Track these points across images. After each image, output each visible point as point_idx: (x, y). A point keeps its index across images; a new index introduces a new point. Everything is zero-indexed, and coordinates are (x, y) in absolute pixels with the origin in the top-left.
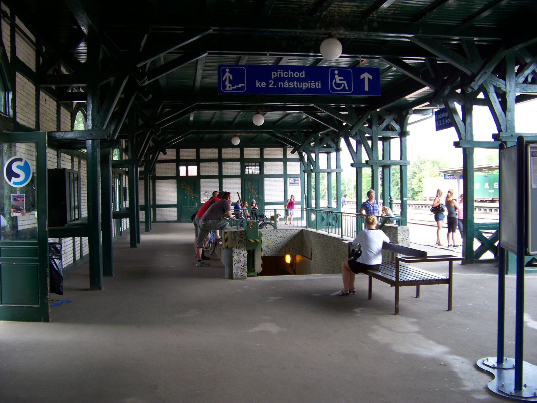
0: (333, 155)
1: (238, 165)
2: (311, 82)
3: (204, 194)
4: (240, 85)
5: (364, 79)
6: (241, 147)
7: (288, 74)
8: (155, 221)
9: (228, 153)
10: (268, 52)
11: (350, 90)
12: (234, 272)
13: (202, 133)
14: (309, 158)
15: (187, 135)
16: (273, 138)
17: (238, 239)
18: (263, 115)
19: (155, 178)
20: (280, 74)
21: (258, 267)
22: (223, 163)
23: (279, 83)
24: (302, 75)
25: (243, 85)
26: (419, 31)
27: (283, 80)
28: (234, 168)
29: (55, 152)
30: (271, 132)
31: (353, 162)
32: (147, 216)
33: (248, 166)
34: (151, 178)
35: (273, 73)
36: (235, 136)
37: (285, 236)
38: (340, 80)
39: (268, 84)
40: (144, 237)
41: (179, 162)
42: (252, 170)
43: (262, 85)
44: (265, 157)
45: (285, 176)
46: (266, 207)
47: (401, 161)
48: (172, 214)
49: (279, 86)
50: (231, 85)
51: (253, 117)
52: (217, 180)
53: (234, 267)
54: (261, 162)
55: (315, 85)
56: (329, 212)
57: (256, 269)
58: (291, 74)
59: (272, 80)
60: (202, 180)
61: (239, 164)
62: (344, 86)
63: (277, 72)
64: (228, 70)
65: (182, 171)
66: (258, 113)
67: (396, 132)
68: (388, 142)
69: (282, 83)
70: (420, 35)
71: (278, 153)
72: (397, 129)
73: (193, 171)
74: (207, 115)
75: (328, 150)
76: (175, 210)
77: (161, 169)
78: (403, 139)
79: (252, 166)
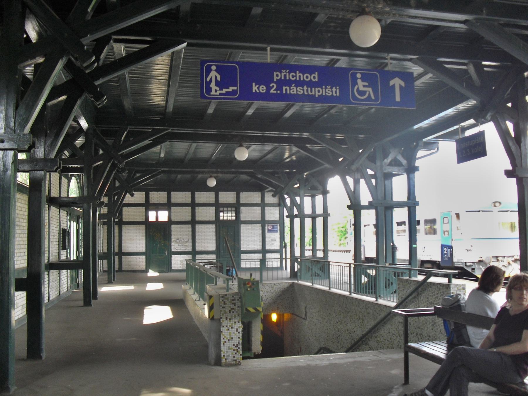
0: (319, 199)
1: (212, 209)
2: (326, 88)
3: (175, 241)
4: (231, 89)
5: (394, 86)
6: (216, 190)
7: (296, 76)
8: (120, 270)
9: (202, 197)
10: (268, 43)
11: (376, 100)
12: (222, 354)
13: (176, 172)
14: (293, 202)
15: (157, 175)
16: (253, 180)
17: (229, 306)
18: (248, 148)
19: (121, 223)
20: (285, 76)
21: (257, 346)
22: (196, 208)
23: (284, 88)
24: (314, 78)
25: (235, 88)
26: (482, 11)
27: (289, 83)
28: (208, 213)
29: (58, 210)
30: (251, 172)
31: (349, 204)
32: (111, 265)
33: (223, 212)
34: (115, 221)
35: (275, 74)
36: (211, 177)
37: (272, 291)
38: (364, 86)
39: (269, 88)
40: (104, 289)
41: (148, 206)
42: (227, 216)
43: (261, 89)
44: (242, 201)
45: (263, 222)
46: (243, 256)
47: (409, 201)
48: (141, 262)
49: (284, 92)
50: (218, 88)
51: (234, 150)
52: (190, 226)
53: (223, 348)
54: (237, 207)
55: (332, 91)
56: (314, 261)
57: (253, 348)
58: (300, 76)
59: (275, 83)
60: (173, 227)
61: (213, 208)
62: (369, 94)
63: (281, 72)
64: (214, 68)
65: (152, 216)
66: (241, 145)
67: (402, 167)
68: (390, 181)
69: (288, 88)
70: (484, 16)
71: (255, 197)
72: (404, 164)
73: (163, 216)
74: (181, 148)
75: (314, 192)
76: (143, 258)
77: (128, 214)
78: (411, 176)
79: (228, 211)
